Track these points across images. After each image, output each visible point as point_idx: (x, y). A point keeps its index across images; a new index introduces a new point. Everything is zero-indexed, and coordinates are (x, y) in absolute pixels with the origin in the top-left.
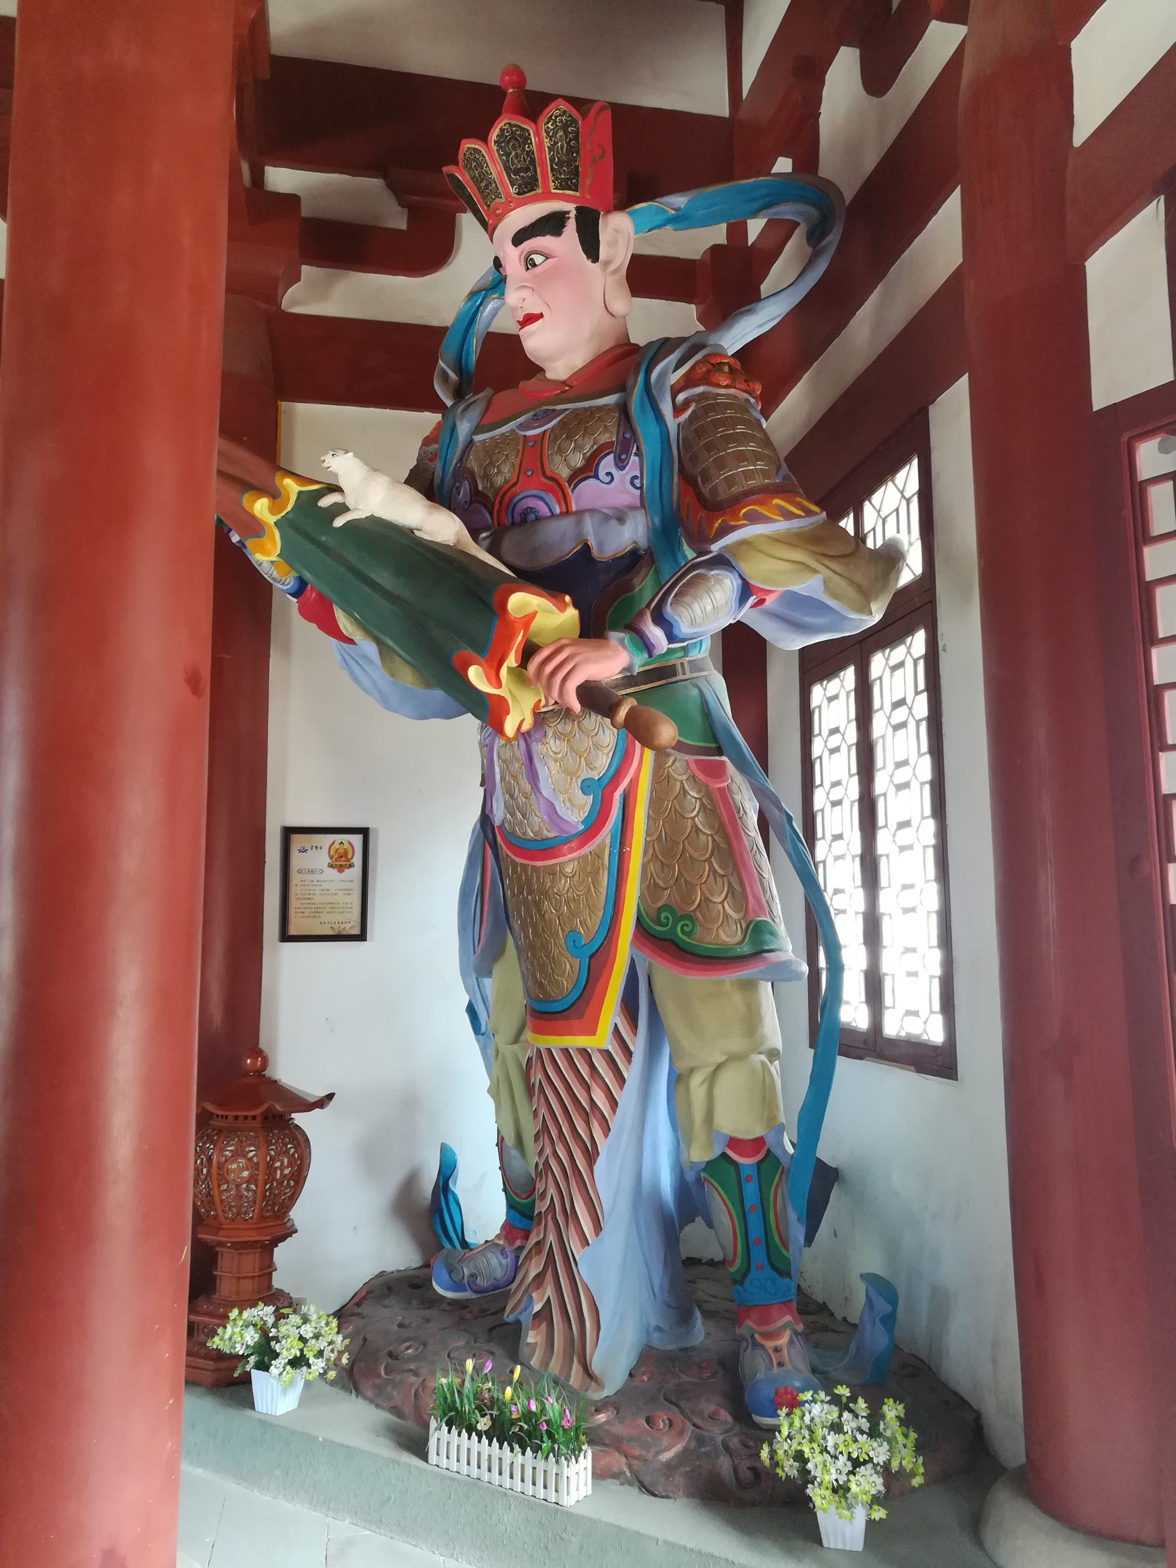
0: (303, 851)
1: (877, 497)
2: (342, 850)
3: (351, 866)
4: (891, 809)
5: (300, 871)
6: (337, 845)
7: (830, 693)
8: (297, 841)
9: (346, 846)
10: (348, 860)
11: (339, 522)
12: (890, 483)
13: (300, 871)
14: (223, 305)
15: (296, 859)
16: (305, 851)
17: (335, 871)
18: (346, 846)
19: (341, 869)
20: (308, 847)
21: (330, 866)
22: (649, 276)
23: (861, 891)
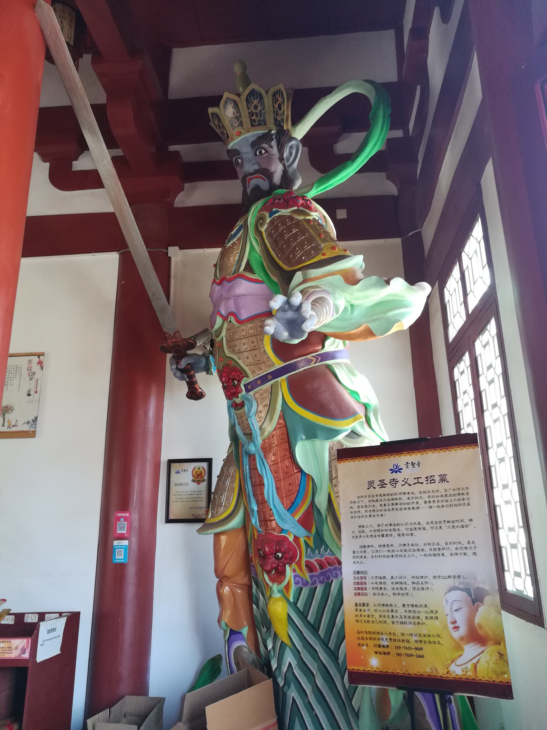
0: (178, 472)
1: (466, 249)
2: (199, 472)
3: (204, 481)
4: (488, 400)
5: (176, 485)
6: (196, 469)
7: (461, 371)
8: (174, 466)
9: (201, 469)
10: (202, 478)
11: (437, 12)
12: (471, 237)
13: (176, 485)
14: (195, 145)
15: (174, 477)
16: (179, 473)
17: (195, 484)
18: (201, 469)
19: (198, 482)
20: (180, 471)
21: (193, 481)
22: (310, 215)
23: (497, 503)
